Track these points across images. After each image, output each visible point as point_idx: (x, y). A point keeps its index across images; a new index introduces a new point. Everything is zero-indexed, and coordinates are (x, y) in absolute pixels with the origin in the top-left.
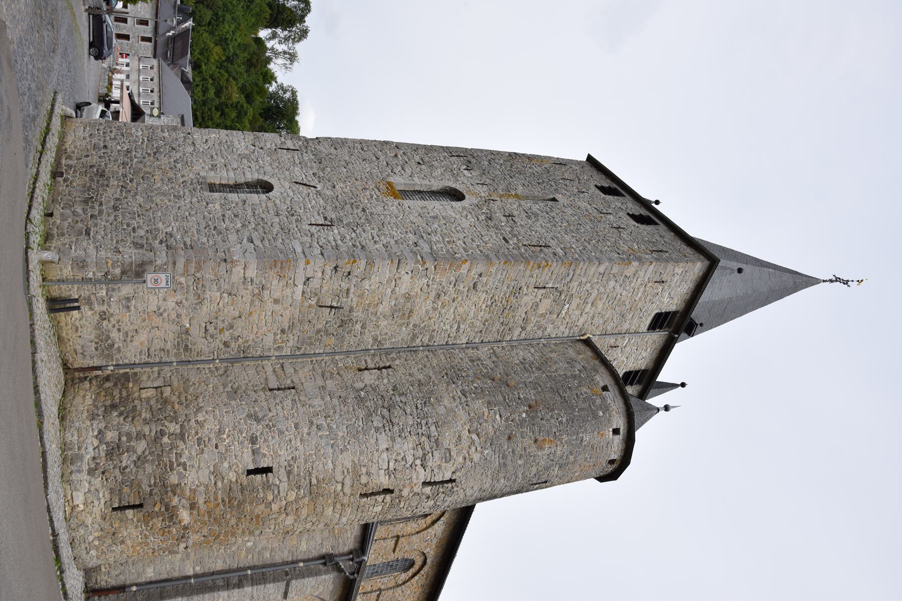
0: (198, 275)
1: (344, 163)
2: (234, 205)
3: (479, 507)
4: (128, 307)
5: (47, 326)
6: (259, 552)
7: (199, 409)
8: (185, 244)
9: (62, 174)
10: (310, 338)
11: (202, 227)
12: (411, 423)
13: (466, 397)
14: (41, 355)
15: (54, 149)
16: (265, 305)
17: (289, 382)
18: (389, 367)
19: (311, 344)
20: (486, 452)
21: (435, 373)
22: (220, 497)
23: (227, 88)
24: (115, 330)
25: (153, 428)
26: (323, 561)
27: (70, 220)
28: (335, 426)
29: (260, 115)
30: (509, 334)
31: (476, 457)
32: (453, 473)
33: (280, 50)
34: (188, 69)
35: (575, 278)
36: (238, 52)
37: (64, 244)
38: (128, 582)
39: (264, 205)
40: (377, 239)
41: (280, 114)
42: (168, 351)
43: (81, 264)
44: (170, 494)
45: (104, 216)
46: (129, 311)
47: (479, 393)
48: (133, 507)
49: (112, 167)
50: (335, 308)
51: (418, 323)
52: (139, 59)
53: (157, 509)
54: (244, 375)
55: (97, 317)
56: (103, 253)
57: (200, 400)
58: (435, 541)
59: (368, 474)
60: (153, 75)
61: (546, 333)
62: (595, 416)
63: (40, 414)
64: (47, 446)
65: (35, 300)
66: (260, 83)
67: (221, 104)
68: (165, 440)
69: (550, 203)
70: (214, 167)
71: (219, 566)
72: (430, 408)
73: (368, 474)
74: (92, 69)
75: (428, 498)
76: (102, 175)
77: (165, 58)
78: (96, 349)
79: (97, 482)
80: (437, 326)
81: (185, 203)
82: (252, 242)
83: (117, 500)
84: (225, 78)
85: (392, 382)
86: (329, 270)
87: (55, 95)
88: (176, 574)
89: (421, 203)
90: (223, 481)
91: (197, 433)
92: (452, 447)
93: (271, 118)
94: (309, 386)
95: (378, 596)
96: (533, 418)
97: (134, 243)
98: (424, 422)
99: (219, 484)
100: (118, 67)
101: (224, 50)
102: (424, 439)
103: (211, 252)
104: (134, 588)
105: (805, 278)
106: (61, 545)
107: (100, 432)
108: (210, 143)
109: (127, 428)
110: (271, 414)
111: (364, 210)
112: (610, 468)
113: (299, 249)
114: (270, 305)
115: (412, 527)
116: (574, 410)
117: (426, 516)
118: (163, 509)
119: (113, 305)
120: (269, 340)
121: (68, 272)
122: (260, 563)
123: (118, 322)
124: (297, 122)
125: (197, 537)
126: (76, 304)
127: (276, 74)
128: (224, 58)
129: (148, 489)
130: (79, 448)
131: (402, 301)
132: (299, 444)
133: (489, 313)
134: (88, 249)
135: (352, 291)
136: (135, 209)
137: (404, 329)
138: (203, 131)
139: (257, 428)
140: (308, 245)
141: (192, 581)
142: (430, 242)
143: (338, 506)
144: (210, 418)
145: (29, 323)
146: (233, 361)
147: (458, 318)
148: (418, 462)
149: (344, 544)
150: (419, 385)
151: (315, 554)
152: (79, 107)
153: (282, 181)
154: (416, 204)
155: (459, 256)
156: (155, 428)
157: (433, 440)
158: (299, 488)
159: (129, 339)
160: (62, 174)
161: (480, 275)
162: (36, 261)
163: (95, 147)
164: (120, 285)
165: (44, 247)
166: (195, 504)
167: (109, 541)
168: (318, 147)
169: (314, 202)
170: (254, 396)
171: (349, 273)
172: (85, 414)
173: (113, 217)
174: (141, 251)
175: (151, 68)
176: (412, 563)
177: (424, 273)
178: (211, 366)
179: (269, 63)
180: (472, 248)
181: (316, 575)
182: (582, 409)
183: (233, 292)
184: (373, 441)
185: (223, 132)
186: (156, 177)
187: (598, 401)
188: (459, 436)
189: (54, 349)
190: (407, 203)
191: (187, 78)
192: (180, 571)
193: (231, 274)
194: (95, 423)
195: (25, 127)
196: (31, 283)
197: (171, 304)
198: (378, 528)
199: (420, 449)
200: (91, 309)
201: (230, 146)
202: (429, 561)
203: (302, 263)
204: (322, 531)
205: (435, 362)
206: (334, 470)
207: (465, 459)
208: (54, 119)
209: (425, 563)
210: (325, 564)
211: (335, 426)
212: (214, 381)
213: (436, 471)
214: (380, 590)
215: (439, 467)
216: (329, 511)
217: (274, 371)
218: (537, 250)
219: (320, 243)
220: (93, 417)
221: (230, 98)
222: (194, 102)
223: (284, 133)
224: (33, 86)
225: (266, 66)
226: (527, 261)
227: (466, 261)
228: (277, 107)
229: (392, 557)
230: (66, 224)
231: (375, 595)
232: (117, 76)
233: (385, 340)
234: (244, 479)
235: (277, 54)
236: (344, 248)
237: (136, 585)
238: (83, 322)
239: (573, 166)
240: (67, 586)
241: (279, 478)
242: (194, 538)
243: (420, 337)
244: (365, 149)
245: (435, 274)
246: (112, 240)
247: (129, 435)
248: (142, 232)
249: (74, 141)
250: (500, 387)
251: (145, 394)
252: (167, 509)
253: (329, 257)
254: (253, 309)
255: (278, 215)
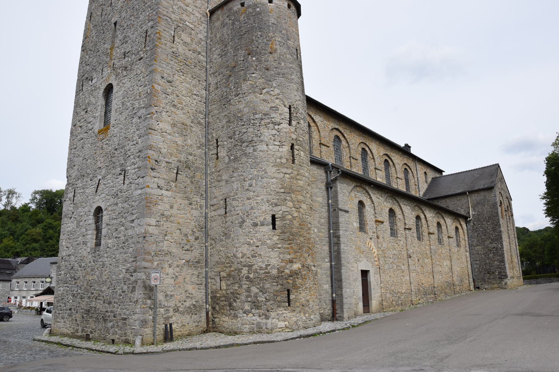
0: (153, 254)
1: (84, 161)
2: (109, 231)
3: (307, 93)
4: (171, 296)
5: (181, 342)
6: (321, 225)
7: (235, 256)
8: (133, 261)
9: (88, 335)
10: (196, 188)
11: (123, 251)
12: (252, 129)
13: (239, 94)
14: (198, 345)
15: (71, 339)
16: (173, 214)
17: (222, 202)
18: (217, 140)
19: (199, 187)
20: (274, 85)
21: (223, 112)
22: (287, 246)
23: (33, 235)
24: (185, 303)
25: (244, 282)
26: (329, 189)
27: (117, 330)
28: (251, 176)
29: (52, 214)
30: (202, 63)
31: (277, 91)
32: (285, 106)
33: (6, 200)
34: (19, 260)
35: (169, 16)
36: (7, 228)
37: (132, 333)
38: (330, 298)
39: (110, 213)
40: (135, 142)
41: (51, 202)
42: (199, 273)
43: (144, 323)
44: (283, 274)
45: (115, 309)
46: (174, 295)
47: (237, 85)
48: (289, 295)
49: (83, 305)
50: (178, 171)
51: (190, 120)
52: (12, 290)
53: (291, 282)
54: (216, 228)
55: (177, 314)
56: (137, 310)
57: (229, 255)
58: (325, 122)
59: (281, 158)
60: (23, 282)
61: (204, 39)
62: (260, 13)
63: (232, 345)
64: (251, 341)
65: (165, 349)
66: (29, 214)
67: (44, 239)
68: (251, 276)
69: (117, 27)
70: (85, 243)
71: (326, 248)
72: (245, 117)
73: (281, 158)
74: (17, 319)
75: (298, 123)
76: (89, 311)
77: (11, 274)
78: (196, 314)
79: (273, 314)
80: (193, 108)
81: (107, 261)
82: (133, 220)
83: (284, 304)
84: (26, 236)
85: (226, 138)
86: (153, 174)
87: (36, 340)
88: (329, 272)
89: (113, 113)
90: (278, 244)
91: (249, 258)
92: (269, 106)
93: (54, 207)
94: (225, 190)
95: (353, 158)
96: (256, 53)
97: (132, 292)
98: (252, 122)
99: (280, 246)
100: (18, 303)
101: (6, 237)
102: (263, 122)
103: (139, 246)
104: (334, 295)
105: (461, 174)
106: (306, 333)
107: (244, 313)
108: (69, 245)
109: (243, 298)
110: (241, 214)
111: (116, 150)
112: (293, 8)
113: (139, 192)
114: (174, 211)
115: (315, 135)
116: (254, 26)
117: (309, 126)
118: (291, 278)
119: (169, 304)
120: (196, 213)
121: (148, 330)
122: (327, 225)
123: (180, 302)
124: (57, 191)
125: (309, 260)
126: (168, 326)
127: (23, 203)
128: (12, 237)
129: (279, 286)
130: (253, 324)
131: (176, 129)
132: (259, 198)
133: (188, 74)
134: (135, 319)
135: (168, 160)
136: (110, 291)
137: (194, 129)
138: (60, 249)
139: (248, 222)
140: (137, 186)
141: (333, 263)
142: (139, 108)
143: (298, 177)
144: (240, 250)
145: (178, 351)
146: (207, 235)
147: (189, 94)
148: (276, 127)
149: (321, 175)
150: (230, 122)
151: (325, 193)
152: (44, 326)
153: (95, 201)
154: (113, 116)
155: (149, 90)
156: (244, 282)
157: (264, 117)
158: (285, 200)
159: (191, 296)
160: (88, 335)
161: (163, 78)
162: (142, 348)
163: (70, 315)
164: (158, 301)
165: (133, 344)
166: (290, 260)
167: (307, 308)
168: (73, 177)
169: (109, 181)
170: (229, 223)
171: (156, 161)
172: (234, 321)
173: (115, 305)
174: (137, 287)
175: (18, 283)
176: (337, 137)
177: (159, 114)
178: (209, 248)
179: (16, 208)
180: (145, 81)
181: (337, 193)
182: (254, 21)
183: (165, 233)
184: (261, 154)
185: (62, 237)
186: (90, 279)
187: (250, 10)
188: (263, 100)
189: (195, 338)
190: (112, 121)
191: (25, 260)
192: (327, 270)
193: (153, 234)
194: (239, 315)
195: (56, 356)
196: (154, 351)
197: (170, 271)
198: (314, 155)
199: (269, 125)
200: (172, 317)
201: (71, 233)
202: (337, 127)
203: (148, 190)
204: (312, 188)
205: (216, 112)
206: (277, 178)
207: (277, 98)
208: (52, 340)
209: (337, 129)
210: (331, 188)
211: (251, 176)
212: (218, 247)
213: (283, 117)
214: (350, 157)
215: (281, 114)
216: (301, 183)
217: (215, 210)
218: (149, 39)
219: (136, 178)
220: (236, 316)
221: (40, 234)
222: (42, 256)
223: (63, 200)
224: (29, 353)
225: (17, 210)
226: (156, 46)
227: (153, 86)
228: (46, 203)
229: (332, 148)
230: (119, 332)
231: (352, 160)
232: (24, 304)
233: (200, 142)
234: (278, 231)
235: (8, 203)
236: (140, 164)
237: (332, 294)
238: (179, 322)
239: (93, 8)
240: (329, 330)
241: (279, 211)
242: (309, 262)
243: (199, 119)
244: (75, 146)
245: (160, 106)
246: (129, 305)
247: (247, 297)
248: (125, 287)
249: (66, 328)
250: (235, 72)
251: (224, 287)
252: (292, 276)
253: (145, 173)
254: (175, 222)
255: (117, 204)
